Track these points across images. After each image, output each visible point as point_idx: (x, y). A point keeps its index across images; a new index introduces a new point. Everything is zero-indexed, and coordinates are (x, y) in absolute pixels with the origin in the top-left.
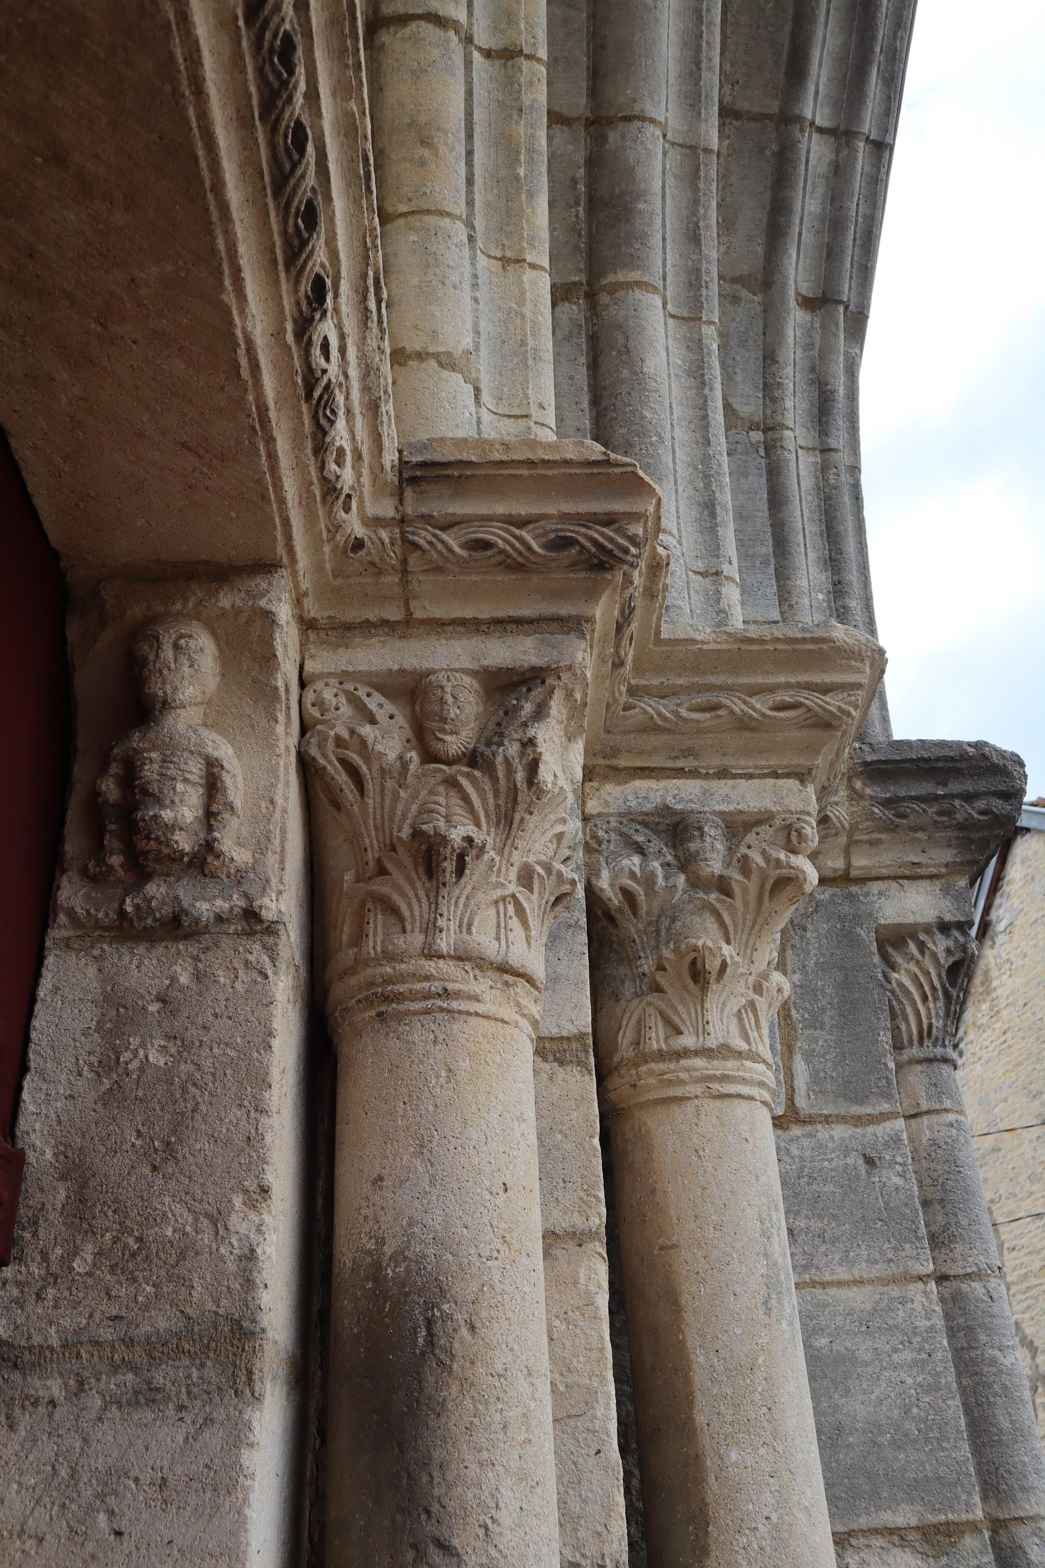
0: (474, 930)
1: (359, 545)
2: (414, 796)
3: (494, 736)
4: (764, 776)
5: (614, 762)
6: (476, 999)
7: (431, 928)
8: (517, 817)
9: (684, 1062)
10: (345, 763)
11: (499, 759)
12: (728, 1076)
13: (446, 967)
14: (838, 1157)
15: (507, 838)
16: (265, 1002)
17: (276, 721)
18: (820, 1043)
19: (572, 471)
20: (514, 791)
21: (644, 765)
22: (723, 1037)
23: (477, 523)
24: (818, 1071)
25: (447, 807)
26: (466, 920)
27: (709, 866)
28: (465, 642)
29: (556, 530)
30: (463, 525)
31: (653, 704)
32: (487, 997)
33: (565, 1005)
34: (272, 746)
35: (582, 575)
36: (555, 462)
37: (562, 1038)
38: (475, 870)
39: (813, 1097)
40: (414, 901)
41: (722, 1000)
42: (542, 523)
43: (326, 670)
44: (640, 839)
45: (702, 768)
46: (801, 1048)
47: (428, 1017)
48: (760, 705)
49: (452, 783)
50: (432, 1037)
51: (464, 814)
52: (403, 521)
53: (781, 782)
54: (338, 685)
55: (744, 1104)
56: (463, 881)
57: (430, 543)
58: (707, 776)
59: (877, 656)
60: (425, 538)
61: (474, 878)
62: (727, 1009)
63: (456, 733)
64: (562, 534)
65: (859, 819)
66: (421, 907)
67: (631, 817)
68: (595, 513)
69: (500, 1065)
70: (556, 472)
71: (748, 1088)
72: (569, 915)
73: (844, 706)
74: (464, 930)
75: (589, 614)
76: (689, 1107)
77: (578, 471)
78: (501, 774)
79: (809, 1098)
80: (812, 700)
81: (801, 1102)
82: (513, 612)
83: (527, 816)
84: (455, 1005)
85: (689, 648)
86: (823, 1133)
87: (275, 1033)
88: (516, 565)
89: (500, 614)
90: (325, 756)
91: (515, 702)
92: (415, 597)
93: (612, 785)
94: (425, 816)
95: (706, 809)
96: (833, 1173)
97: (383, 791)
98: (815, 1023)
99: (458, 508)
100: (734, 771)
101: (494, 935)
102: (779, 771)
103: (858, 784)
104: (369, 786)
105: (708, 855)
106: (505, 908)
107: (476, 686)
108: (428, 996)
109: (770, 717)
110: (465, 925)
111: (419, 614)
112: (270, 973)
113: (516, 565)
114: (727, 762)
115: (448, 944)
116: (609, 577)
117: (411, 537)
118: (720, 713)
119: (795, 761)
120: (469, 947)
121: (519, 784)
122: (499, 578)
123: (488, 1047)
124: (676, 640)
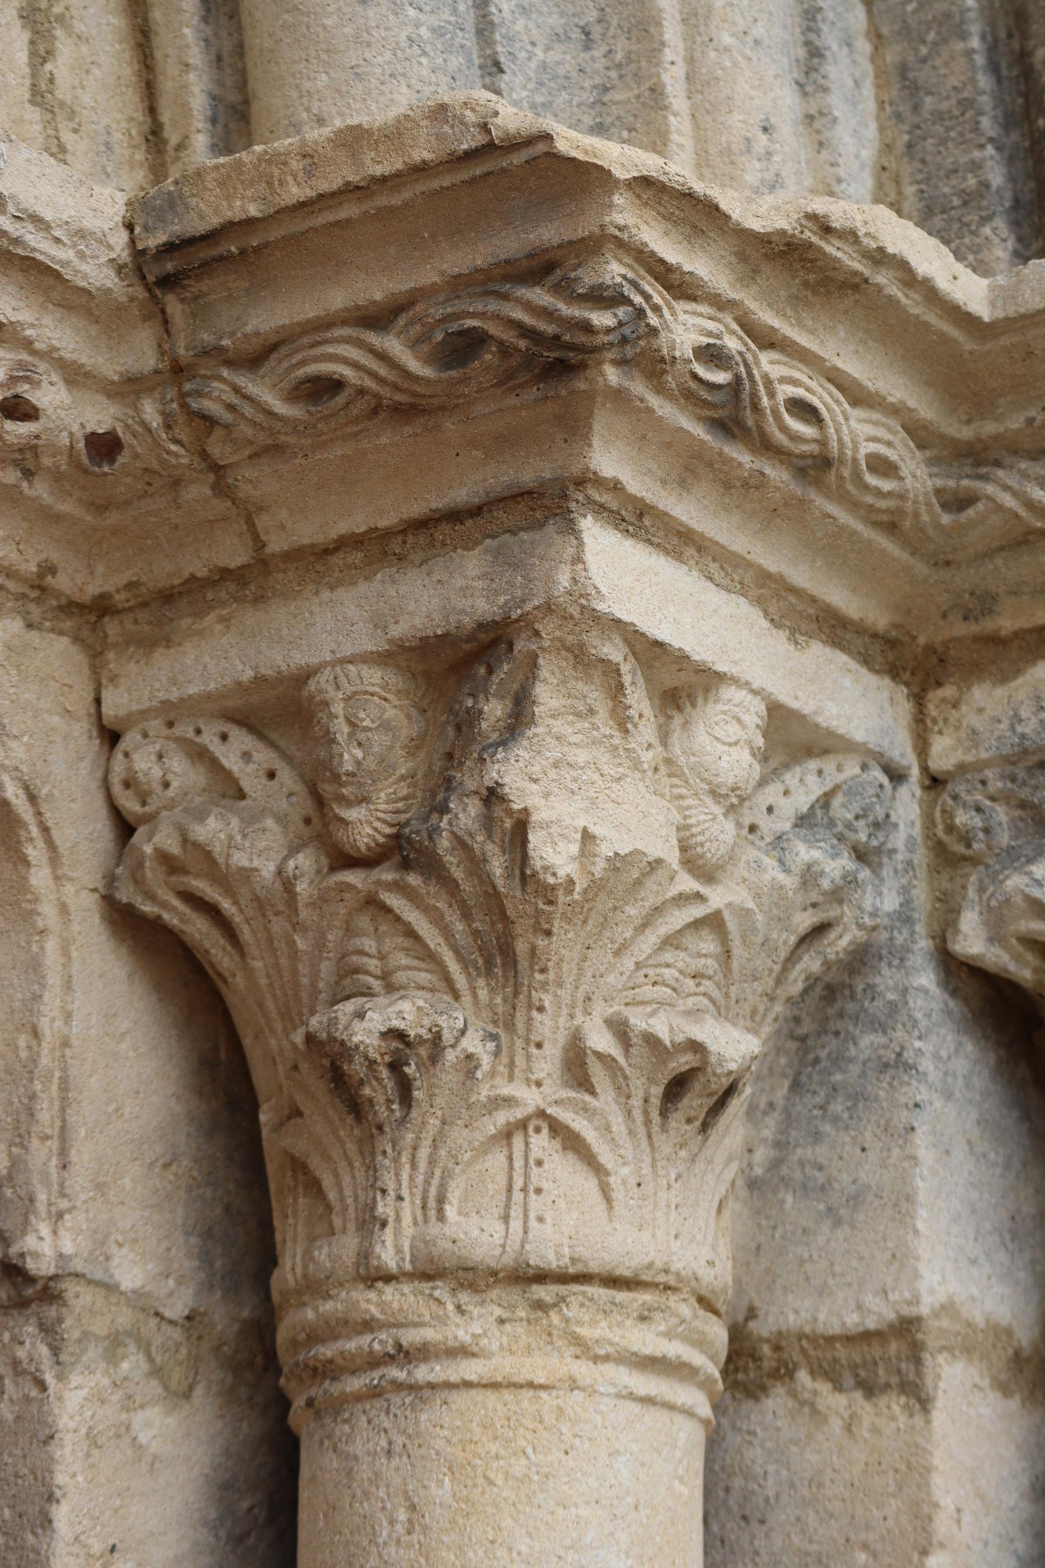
0: (450, 1211)
1: (104, 446)
2: (320, 945)
3: (437, 793)
5: (989, 625)
6: (463, 1352)
7: (370, 1222)
8: (521, 947)
10: (191, 898)
11: (444, 843)
13: (395, 1297)
15: (516, 993)
16: (42, 1436)
17: (27, 863)
19: (435, 184)
20: (493, 899)
23: (306, 340)
25: (382, 957)
26: (433, 1191)
28: (362, 587)
29: (444, 320)
30: (283, 350)
31: (1013, 483)
32: (493, 1343)
34: (29, 916)
35: (533, 393)
36: (398, 175)
37: (867, 1336)
38: (436, 1091)
40: (343, 1164)
42: (419, 307)
43: (134, 707)
47: (380, 1403)
49: (373, 904)
50: (383, 1443)
51: (415, 963)
52: (178, 370)
54: (165, 731)
56: (414, 1114)
57: (231, 407)
60: (219, 399)
61: (439, 1101)
63: (365, 800)
64: (454, 327)
66: (354, 1177)
68: (507, 262)
69: (525, 1479)
70: (407, 194)
74: (432, 1213)
75: (576, 470)
77: (446, 181)
78: (458, 873)
82: (439, 502)
83: (541, 942)
84: (422, 1373)
87: (58, 1493)
88: (408, 408)
89: (416, 509)
90: (151, 897)
91: (470, 703)
92: (261, 509)
93: (987, 686)
94: (347, 981)
97: (270, 940)
99: (264, 319)
101: (498, 1212)
104: (246, 934)
106: (527, 1144)
107: (394, 679)
108: (374, 1362)
110: (432, 1203)
111: (276, 544)
112: (49, 1378)
113: (408, 408)
115: (399, 1250)
116: (582, 385)
117: (194, 404)
120: (436, 1251)
121: (500, 883)
122: (384, 440)
123: (494, 1448)
124: (1024, 317)
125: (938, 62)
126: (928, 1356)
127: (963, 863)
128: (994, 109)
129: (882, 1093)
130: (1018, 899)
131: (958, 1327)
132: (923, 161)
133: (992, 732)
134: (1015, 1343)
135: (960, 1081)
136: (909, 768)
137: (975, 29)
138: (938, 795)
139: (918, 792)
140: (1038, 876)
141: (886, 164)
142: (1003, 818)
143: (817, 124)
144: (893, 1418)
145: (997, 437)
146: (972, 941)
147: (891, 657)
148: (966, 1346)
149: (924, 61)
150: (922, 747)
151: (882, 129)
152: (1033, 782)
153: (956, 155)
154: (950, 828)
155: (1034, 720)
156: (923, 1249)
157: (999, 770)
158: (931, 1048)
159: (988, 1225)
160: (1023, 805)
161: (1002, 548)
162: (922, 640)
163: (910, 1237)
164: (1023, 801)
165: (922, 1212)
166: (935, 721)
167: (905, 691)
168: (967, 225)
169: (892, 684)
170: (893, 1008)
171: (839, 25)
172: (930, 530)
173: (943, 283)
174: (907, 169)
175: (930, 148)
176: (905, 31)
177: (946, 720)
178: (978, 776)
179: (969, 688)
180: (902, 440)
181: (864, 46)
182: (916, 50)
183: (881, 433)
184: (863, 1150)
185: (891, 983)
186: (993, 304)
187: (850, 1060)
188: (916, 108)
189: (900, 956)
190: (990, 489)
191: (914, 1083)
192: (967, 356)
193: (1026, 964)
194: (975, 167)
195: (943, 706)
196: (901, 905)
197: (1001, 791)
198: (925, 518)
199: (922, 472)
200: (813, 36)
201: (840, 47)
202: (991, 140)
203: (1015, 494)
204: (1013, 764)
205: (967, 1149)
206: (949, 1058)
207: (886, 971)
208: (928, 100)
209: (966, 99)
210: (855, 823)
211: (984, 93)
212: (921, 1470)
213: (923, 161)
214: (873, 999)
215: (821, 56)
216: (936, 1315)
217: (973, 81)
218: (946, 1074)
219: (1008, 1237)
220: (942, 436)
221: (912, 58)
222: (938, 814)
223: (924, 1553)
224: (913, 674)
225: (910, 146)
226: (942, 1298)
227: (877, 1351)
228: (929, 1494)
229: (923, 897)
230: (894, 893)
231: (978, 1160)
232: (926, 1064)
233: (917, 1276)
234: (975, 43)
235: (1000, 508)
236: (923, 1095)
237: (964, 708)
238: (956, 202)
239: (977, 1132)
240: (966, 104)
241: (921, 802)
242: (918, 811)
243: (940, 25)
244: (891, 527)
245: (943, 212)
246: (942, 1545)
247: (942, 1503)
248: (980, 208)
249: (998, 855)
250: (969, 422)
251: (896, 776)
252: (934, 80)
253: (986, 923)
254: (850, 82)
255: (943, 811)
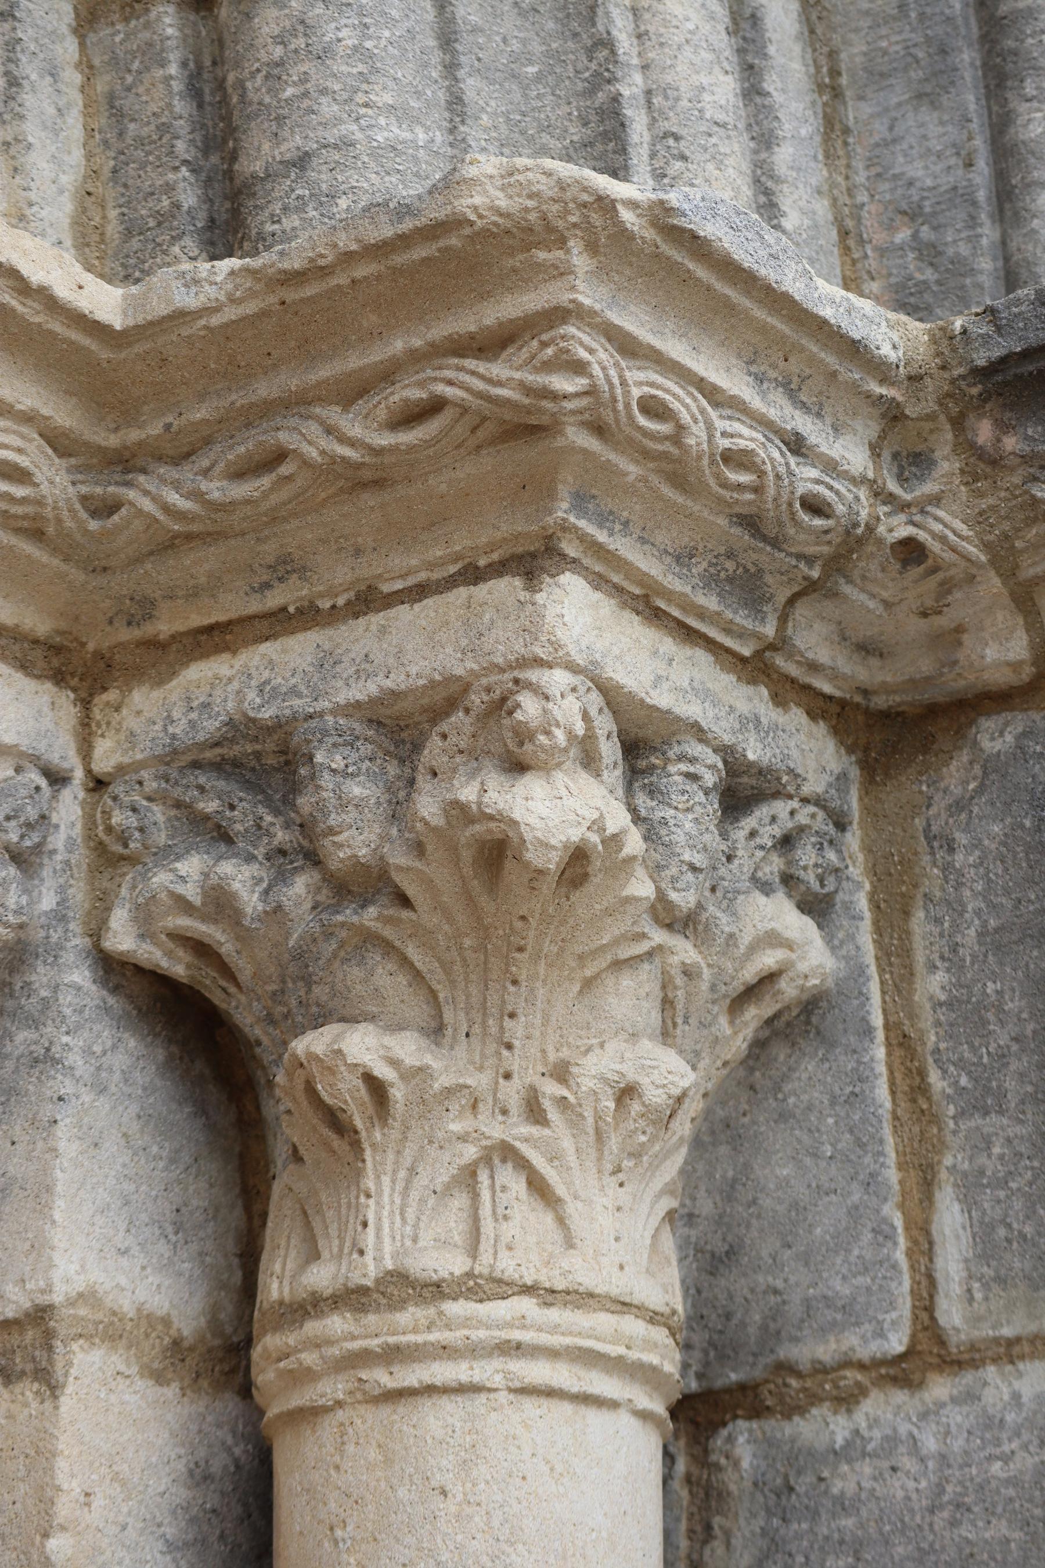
4: (450, 583)
5: (149, 630)
9: (312, 1327)
12: (397, 1348)
14: (1025, 1447)
18: (996, 1150)
21: (207, 621)
22: (395, 1255)
24: (991, 1227)
27: (340, 846)
33: (15, 1248)
39: (978, 1296)
41: (408, 1161)
44: (211, 806)
45: (321, 595)
46: (952, 1169)
48: (363, 430)
53: (481, 591)
55: (451, 1408)
58: (334, 616)
59: (596, 219)
62: (422, 1180)
65: (1006, 526)
67: (189, 758)
71: (464, 1365)
72: (35, 1036)
73: (530, 378)
76: (327, 1428)
79: (971, 1299)
80: (463, 381)
81: (952, 1314)
85: (185, 332)
86: (996, 1385)
93: (145, 689)
95: (324, 704)
96: (1011, 1492)
98: (982, 1100)
100: (386, 588)
102: (482, 562)
103: (984, 431)
105: (333, 820)
109: (393, 449)
114: (367, 569)
118: (285, 470)
119: (505, 529)
124: (151, 324)
125: (141, 90)
126: (59, 1343)
127: (122, 863)
128: (192, 132)
129: (30, 1087)
130: (163, 896)
131: (99, 1316)
132: (125, 186)
133: (147, 733)
134: (173, 1332)
135: (117, 1076)
136: (72, 770)
137: (174, 57)
138: (101, 797)
139: (81, 795)
140: (183, 873)
141: (91, 190)
142: (160, 818)
143: (12, 151)
144: (26, 1405)
145: (140, 444)
146: (123, 938)
147: (55, 662)
148: (111, 1331)
149: (128, 89)
150: (86, 750)
151: (89, 156)
152: (184, 781)
153: (154, 179)
154: (109, 829)
155: (184, 721)
156: (58, 1237)
157: (154, 770)
158: (81, 1043)
159: (144, 1217)
160: (178, 805)
161: (151, 553)
162: (91, 646)
163: (47, 1227)
164: (178, 801)
165: (60, 1203)
166: (99, 726)
167: (72, 696)
168: (159, 245)
169: (55, 689)
170: (45, 1003)
171: (41, 56)
172: (78, 537)
173: (63, 292)
174: (111, 194)
175: (132, 173)
176: (114, 62)
177: (108, 723)
178: (135, 777)
179: (130, 691)
180: (38, 447)
181: (73, 77)
182: (123, 78)
183: (18, 442)
184: (13, 1143)
185: (45, 980)
186: (125, 313)
187: (6, 1057)
188: (121, 134)
189: (54, 953)
190: (132, 494)
191: (60, 1077)
192: (105, 365)
193: (179, 960)
194: (169, 188)
195: (107, 710)
196: (58, 903)
197: (156, 792)
198: (69, 523)
199: (62, 479)
200: (12, 67)
201: (42, 77)
202: (185, 162)
203: (154, 499)
204: (167, 764)
205: (123, 1142)
206: (104, 1053)
207: (41, 969)
208: (132, 126)
209: (163, 124)
210: (5, 824)
211: (181, 118)
212: (48, 1455)
213: (125, 186)
214: (29, 996)
215: (19, 85)
216: (72, 1303)
217: (170, 105)
218: (99, 1068)
219: (170, 1229)
220: (87, 444)
221: (119, 87)
222: (99, 815)
223: (46, 1535)
224: (81, 680)
225: (115, 171)
226: (80, 1285)
227: (15, 1340)
228: (53, 1478)
229: (80, 897)
230: (52, 893)
231: (135, 1154)
232: (74, 1059)
233: (52, 1266)
234: (173, 69)
235: (140, 511)
236: (67, 1088)
237: (125, 711)
238: (152, 223)
239: (135, 1126)
240: (164, 129)
241: (83, 804)
242: (80, 813)
243: (144, 54)
244: (37, 534)
245: (140, 234)
246: (63, 1528)
247: (65, 1487)
248: (171, 229)
249: (155, 854)
250: (116, 430)
251: (57, 779)
252: (137, 107)
253: (135, 919)
254: (52, 111)
255: (103, 812)
